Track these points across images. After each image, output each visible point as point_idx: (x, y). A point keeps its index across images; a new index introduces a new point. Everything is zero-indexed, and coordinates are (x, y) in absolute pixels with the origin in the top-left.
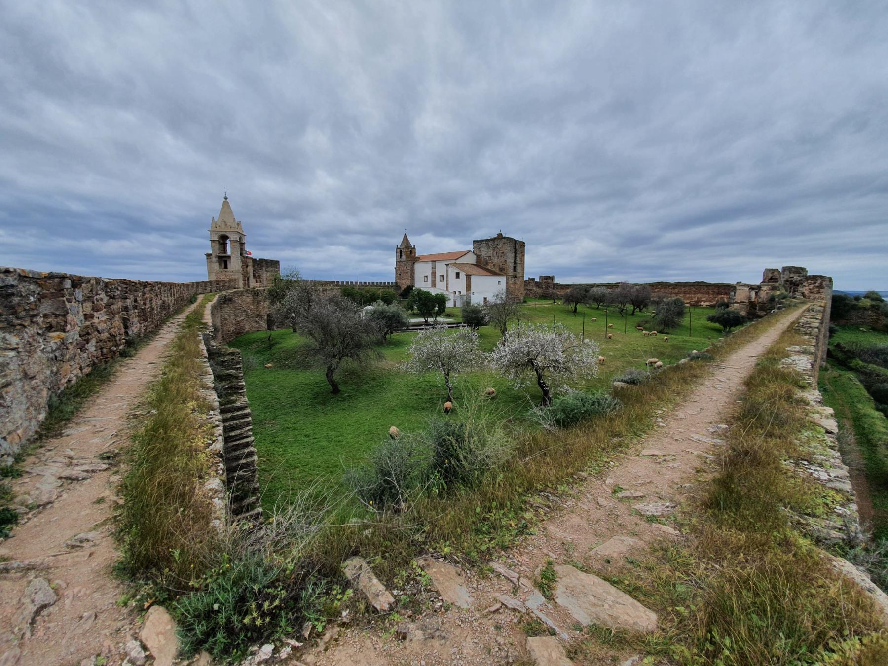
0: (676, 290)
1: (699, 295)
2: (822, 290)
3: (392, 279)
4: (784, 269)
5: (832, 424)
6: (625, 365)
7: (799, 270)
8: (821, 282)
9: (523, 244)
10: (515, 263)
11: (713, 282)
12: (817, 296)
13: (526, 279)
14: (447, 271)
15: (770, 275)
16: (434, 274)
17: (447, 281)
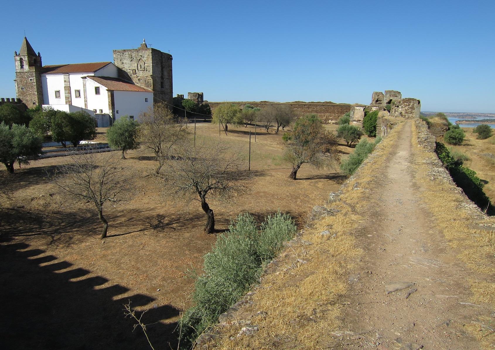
0: (310, 110)
1: (327, 114)
2: (413, 111)
3: (15, 168)
4: (386, 92)
5: (222, 211)
6: (359, 181)
7: (397, 94)
8: (413, 103)
9: (169, 58)
10: (162, 78)
11: (338, 102)
12: (410, 115)
13: (175, 95)
14: (84, 85)
15: (377, 97)
16: (68, 89)
17: (85, 97)
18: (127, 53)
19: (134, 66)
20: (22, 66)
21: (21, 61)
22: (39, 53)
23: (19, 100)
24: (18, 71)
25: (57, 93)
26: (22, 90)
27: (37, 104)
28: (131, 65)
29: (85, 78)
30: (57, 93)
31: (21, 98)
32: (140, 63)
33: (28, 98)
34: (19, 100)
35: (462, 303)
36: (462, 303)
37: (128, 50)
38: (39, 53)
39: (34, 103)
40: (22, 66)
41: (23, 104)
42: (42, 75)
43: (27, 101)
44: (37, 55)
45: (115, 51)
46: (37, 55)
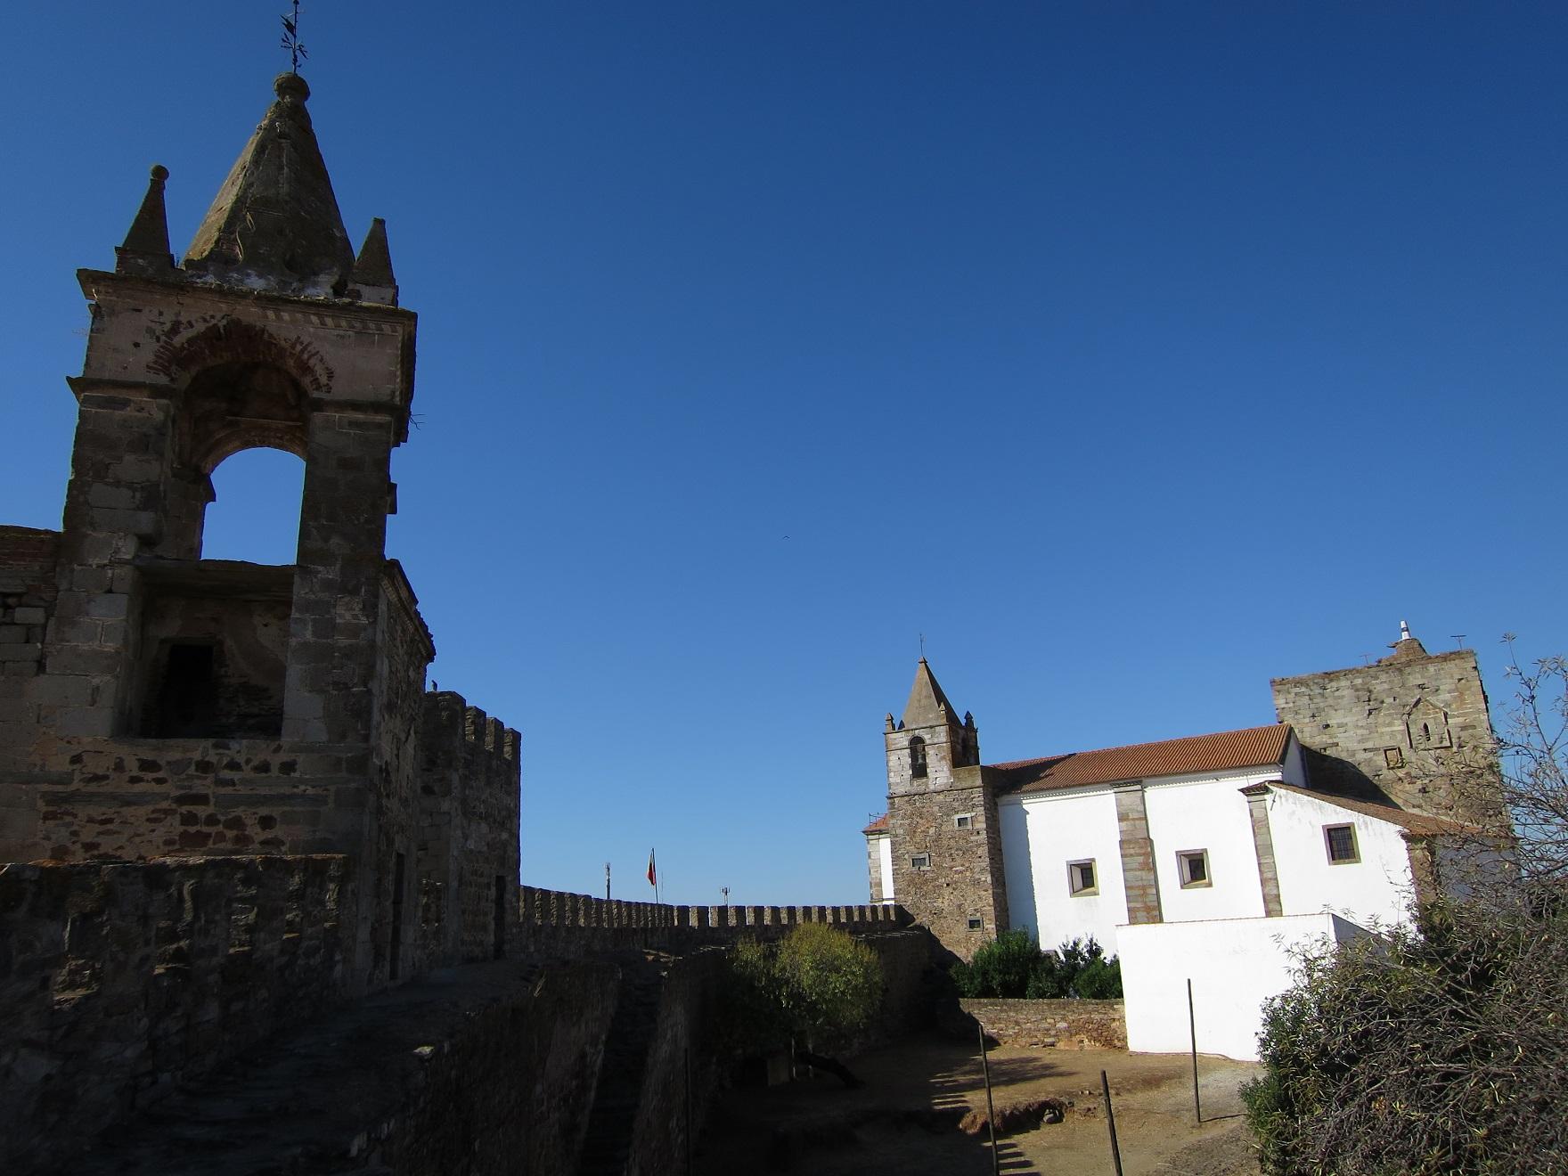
16: (1138, 847)
18: (1344, 683)
19: (1392, 730)
20: (919, 771)
21: (917, 746)
22: (968, 717)
23: (899, 909)
24: (901, 790)
25: (1084, 875)
26: (912, 868)
27: (991, 926)
28: (1372, 730)
29: (1262, 789)
30: (1084, 875)
31: (908, 904)
32: (1419, 719)
33: (945, 902)
34: (899, 909)
35: (188, 917)
36: (188, 917)
37: (1346, 673)
38: (968, 717)
39: (973, 924)
40: (919, 771)
41: (920, 927)
42: (1006, 799)
43: (938, 913)
44: (963, 722)
45: (1278, 684)
46: (963, 722)
